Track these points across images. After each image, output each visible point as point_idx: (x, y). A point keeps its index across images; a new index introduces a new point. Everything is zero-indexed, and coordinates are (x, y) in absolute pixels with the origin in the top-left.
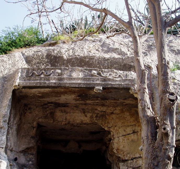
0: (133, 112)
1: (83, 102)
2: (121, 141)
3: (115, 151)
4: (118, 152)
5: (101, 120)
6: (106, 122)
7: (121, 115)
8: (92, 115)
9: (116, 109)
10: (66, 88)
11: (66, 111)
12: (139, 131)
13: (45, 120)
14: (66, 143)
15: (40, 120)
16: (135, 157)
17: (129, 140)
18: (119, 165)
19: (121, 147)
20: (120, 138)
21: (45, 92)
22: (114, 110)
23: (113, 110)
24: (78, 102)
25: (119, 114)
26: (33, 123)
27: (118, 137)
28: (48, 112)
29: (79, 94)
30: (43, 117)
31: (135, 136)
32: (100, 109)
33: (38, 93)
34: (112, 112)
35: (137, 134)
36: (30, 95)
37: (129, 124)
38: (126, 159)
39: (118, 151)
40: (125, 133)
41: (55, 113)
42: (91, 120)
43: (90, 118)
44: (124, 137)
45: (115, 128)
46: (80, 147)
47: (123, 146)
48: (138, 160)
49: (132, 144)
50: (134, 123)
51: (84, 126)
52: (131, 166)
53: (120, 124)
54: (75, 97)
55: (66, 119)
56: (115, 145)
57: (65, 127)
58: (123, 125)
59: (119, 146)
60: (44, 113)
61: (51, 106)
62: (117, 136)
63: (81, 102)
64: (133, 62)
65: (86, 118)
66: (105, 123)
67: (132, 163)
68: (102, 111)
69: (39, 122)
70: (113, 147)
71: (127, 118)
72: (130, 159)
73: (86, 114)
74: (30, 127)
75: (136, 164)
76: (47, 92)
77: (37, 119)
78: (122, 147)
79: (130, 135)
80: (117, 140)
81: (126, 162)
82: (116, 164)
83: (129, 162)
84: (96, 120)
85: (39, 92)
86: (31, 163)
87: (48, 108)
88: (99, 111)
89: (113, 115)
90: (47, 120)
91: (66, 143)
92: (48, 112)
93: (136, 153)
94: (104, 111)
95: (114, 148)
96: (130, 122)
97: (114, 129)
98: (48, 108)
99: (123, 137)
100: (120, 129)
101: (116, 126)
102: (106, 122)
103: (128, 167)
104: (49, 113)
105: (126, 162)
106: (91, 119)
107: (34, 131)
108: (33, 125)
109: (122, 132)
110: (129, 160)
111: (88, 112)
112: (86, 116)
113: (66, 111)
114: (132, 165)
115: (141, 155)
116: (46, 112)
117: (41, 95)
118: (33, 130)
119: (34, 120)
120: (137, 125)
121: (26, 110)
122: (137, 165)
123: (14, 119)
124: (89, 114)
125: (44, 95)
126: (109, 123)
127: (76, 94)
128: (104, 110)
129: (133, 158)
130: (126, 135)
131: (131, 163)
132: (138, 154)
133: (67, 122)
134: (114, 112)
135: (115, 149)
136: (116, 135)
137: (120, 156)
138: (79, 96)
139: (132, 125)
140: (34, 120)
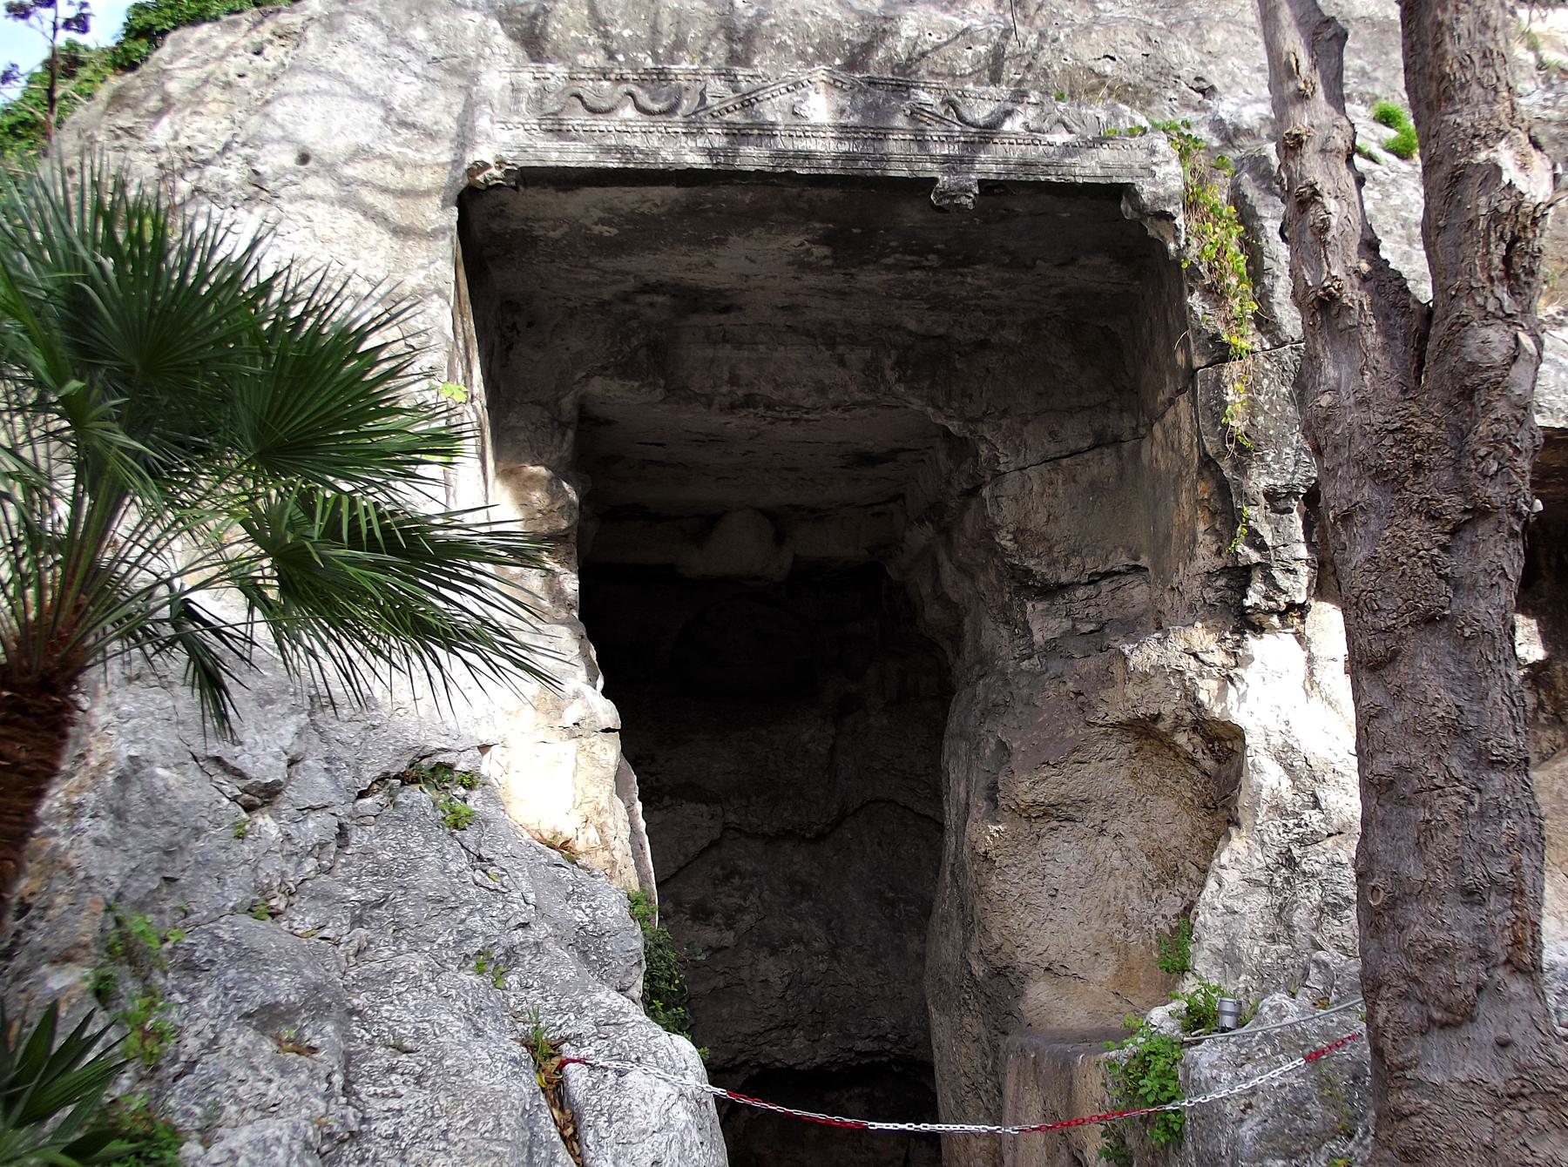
1: (836, 280)
3: (1005, 541)
4: (1022, 548)
10: (773, 184)
12: (1127, 435)
14: (707, 522)
16: (1108, 567)
20: (1032, 472)
21: (643, 214)
24: (810, 280)
27: (1021, 469)
28: (634, 342)
31: (1107, 461)
32: (921, 321)
33: (602, 221)
34: (982, 336)
35: (1118, 451)
36: (552, 234)
38: (1064, 579)
40: (1052, 449)
43: (863, 371)
45: (1004, 422)
49: (1094, 502)
54: (802, 244)
55: (734, 380)
56: (1005, 511)
61: (652, 305)
62: (1012, 466)
63: (824, 281)
64: (1113, 59)
68: (925, 337)
70: (998, 521)
73: (841, 349)
76: (655, 211)
78: (1041, 517)
79: (1079, 458)
80: (1017, 485)
82: (1005, 609)
84: (899, 380)
85: (610, 210)
88: (910, 333)
90: (636, 384)
91: (707, 522)
92: (634, 342)
94: (940, 337)
95: (998, 527)
97: (1000, 427)
100: (1030, 427)
107: (565, 446)
110: (1079, 583)
111: (853, 341)
112: (842, 362)
114: (1092, 611)
115: (1137, 559)
117: (614, 231)
118: (561, 442)
120: (1115, 405)
121: (513, 327)
127: (817, 225)
128: (941, 330)
134: (994, 339)
137: (1031, 563)
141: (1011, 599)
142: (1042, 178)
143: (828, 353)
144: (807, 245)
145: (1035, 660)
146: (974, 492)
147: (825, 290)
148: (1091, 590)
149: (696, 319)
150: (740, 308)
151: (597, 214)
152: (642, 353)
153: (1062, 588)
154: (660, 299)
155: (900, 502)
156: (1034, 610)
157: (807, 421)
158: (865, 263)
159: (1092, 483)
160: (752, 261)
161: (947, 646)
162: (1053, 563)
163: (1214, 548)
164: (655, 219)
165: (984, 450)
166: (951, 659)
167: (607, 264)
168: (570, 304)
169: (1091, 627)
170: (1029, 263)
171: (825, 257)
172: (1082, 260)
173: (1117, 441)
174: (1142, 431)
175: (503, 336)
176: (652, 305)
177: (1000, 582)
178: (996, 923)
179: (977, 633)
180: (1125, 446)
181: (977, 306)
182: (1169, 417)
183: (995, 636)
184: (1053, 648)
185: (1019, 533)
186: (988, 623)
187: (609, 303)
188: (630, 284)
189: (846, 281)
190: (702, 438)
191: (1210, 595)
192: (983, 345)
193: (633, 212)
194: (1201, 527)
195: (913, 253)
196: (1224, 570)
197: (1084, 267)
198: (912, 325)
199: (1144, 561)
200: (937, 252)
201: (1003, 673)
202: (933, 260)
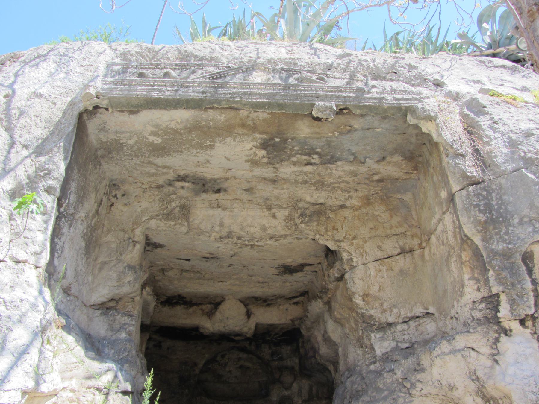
0: (395, 202)
1: (268, 172)
2: (372, 273)
5: (315, 224)
6: (330, 227)
7: (365, 211)
8: (289, 214)
9: (350, 197)
11: (220, 205)
13: (165, 222)
14: (215, 303)
15: (153, 223)
17: (392, 270)
18: (370, 339)
19: (374, 290)
20: (370, 265)
22: (346, 199)
23: (343, 199)
24: (258, 172)
25: (360, 207)
26: (133, 230)
27: (364, 264)
28: (173, 205)
29: (264, 136)
30: (161, 217)
32: (312, 196)
33: (153, 134)
34: (342, 203)
37: (389, 232)
38: (391, 320)
39: (366, 299)
40: (380, 255)
41: (193, 211)
42: (287, 226)
43: (285, 220)
44: (378, 262)
45: (354, 241)
46: (249, 315)
47: (380, 287)
48: (421, 321)
49: (403, 280)
50: (401, 230)
51: (267, 244)
52: (404, 339)
53: (364, 232)
54: (251, 149)
55: (221, 225)
57: (219, 247)
58: (373, 233)
59: (368, 287)
60: (163, 205)
61: (183, 188)
62: (360, 263)
65: (274, 222)
66: (327, 230)
67: (406, 332)
69: (148, 229)
70: (354, 290)
71: (380, 217)
72: (401, 320)
73: (273, 211)
74: (126, 239)
75: (416, 334)
77: (144, 221)
79: (393, 259)
81: (391, 330)
83: (399, 328)
84: (302, 222)
85: (156, 126)
86: (123, 335)
87: (176, 194)
88: (307, 203)
89: (344, 210)
90: (173, 223)
92: (173, 205)
93: (416, 303)
94: (321, 204)
96: (391, 227)
97: (352, 244)
98: (174, 193)
99: (376, 264)
100: (368, 243)
101: (354, 238)
102: (330, 227)
103: (397, 342)
104: (177, 207)
105: (391, 330)
106: (288, 224)
107: (135, 251)
108: (134, 237)
109: (372, 251)
110: (398, 323)
111: (280, 207)
112: (274, 217)
113: (220, 205)
114: (406, 337)
116: (169, 202)
119: (136, 223)
120: (408, 233)
122: (421, 336)
123: (81, 199)
124: (282, 211)
125: (171, 142)
126: (337, 229)
127: (258, 136)
129: (407, 317)
130: (384, 259)
131: (404, 330)
132: (420, 307)
133: (224, 233)
134: (348, 204)
135: (359, 296)
136: (357, 258)
137: (372, 312)
138: (264, 146)
139: (396, 235)
140: (136, 223)
141: (363, 333)
142: (367, 104)
143: (268, 212)
144: (254, 149)
145: (378, 364)
146: (341, 278)
147: (265, 179)
148: (405, 326)
149: (204, 196)
150: (225, 190)
151: (150, 129)
152: (177, 210)
153: (390, 325)
154: (186, 184)
155: (306, 296)
156: (375, 337)
157: (258, 246)
158: (282, 161)
159: (401, 271)
160: (228, 159)
161: (331, 368)
162: (384, 311)
163: (475, 287)
164: (176, 132)
165: (345, 255)
166: (333, 375)
167: (159, 161)
168: (144, 186)
169: (407, 345)
170: (363, 160)
171: (264, 157)
172: (388, 159)
173: (411, 251)
174: (424, 244)
175: (109, 199)
176: (183, 188)
177: (356, 325)
178: (98, 86)
179: (346, 356)
180: (416, 252)
181: (339, 187)
182: (440, 228)
183: (354, 354)
184: (387, 358)
185: (365, 296)
186: (351, 349)
187: (162, 186)
188: (171, 176)
189: (275, 172)
190: (208, 255)
191: (478, 315)
192: (343, 207)
193: (167, 128)
194: (466, 277)
195: (306, 154)
196: (484, 299)
197: (389, 163)
198: (308, 199)
199: (431, 310)
200: (317, 153)
201: (360, 373)
202: (316, 159)
